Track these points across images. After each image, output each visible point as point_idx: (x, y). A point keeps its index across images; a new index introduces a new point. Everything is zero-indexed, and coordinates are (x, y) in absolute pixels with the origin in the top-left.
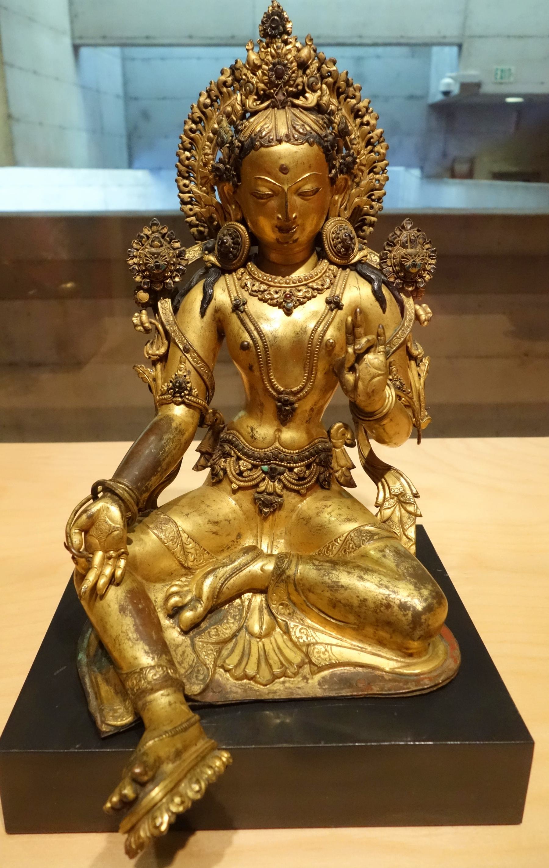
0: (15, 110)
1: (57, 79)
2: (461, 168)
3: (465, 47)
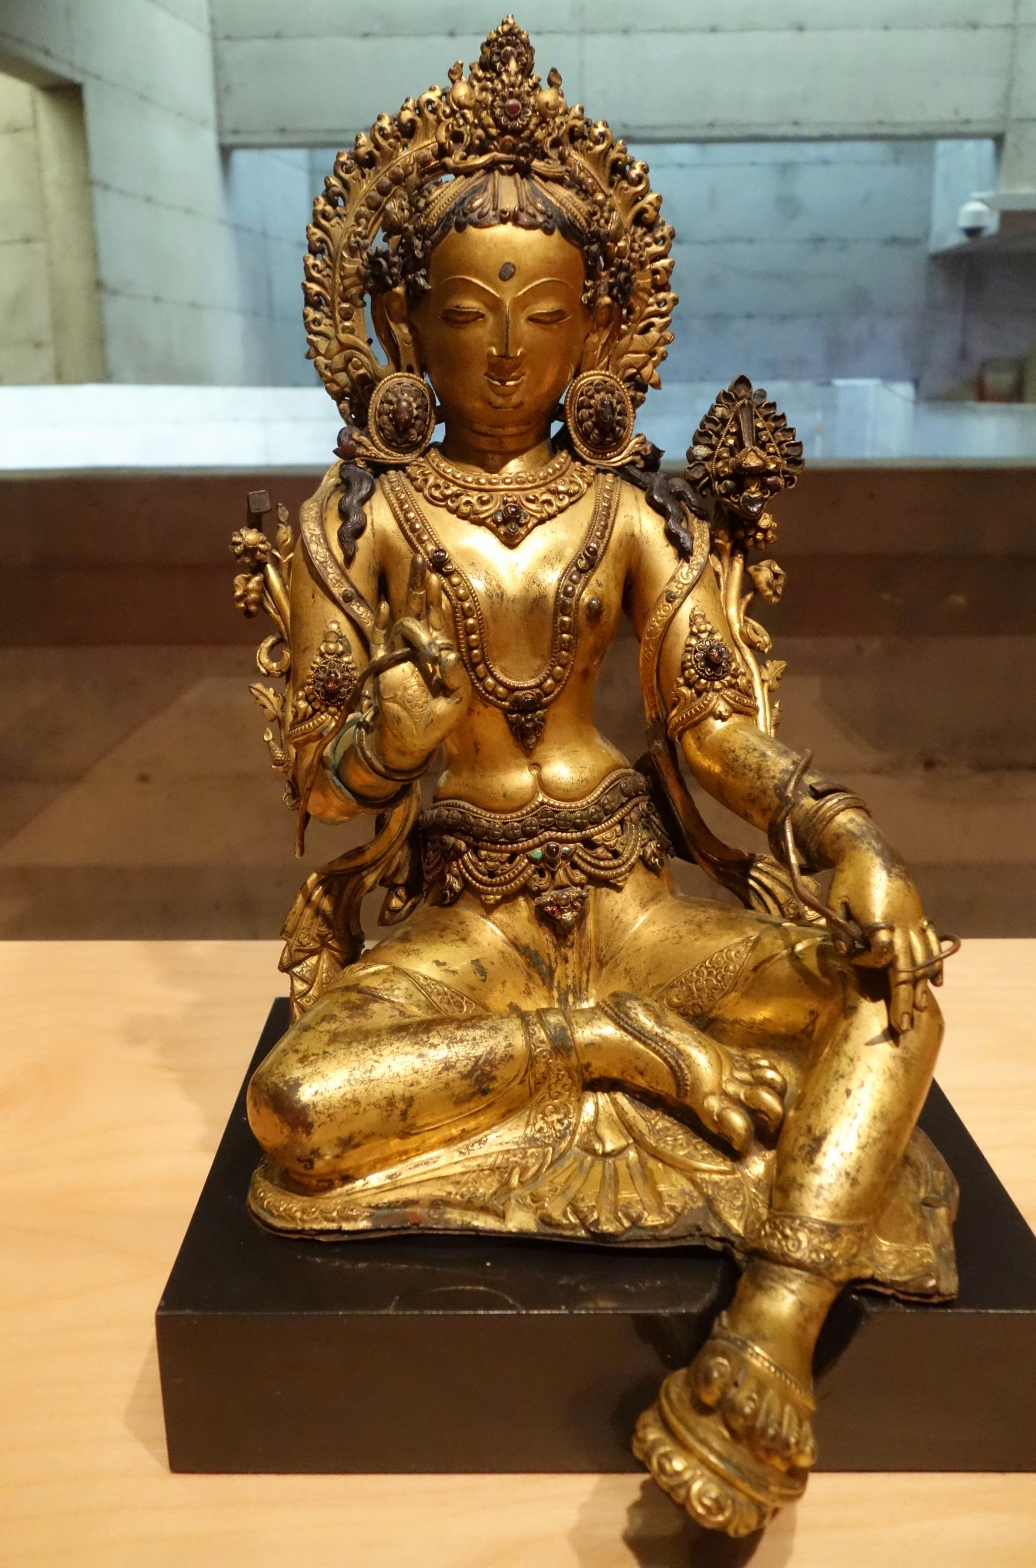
0: (109, 274)
1: (188, 211)
2: (1003, 380)
3: (1010, 139)
